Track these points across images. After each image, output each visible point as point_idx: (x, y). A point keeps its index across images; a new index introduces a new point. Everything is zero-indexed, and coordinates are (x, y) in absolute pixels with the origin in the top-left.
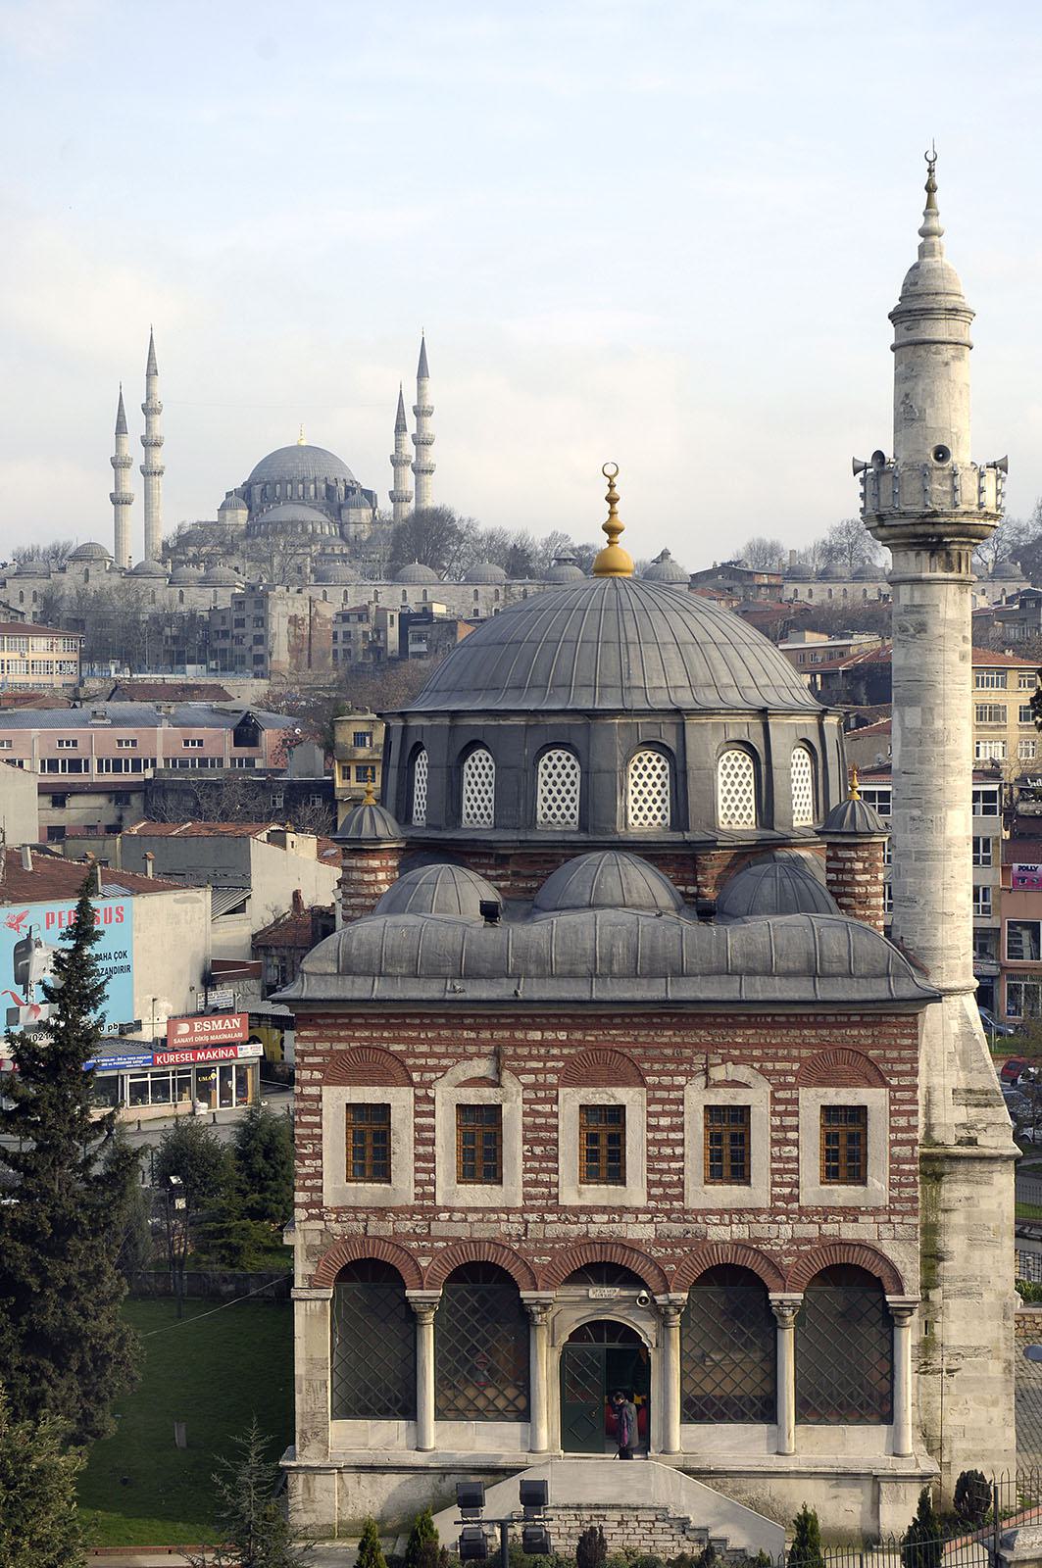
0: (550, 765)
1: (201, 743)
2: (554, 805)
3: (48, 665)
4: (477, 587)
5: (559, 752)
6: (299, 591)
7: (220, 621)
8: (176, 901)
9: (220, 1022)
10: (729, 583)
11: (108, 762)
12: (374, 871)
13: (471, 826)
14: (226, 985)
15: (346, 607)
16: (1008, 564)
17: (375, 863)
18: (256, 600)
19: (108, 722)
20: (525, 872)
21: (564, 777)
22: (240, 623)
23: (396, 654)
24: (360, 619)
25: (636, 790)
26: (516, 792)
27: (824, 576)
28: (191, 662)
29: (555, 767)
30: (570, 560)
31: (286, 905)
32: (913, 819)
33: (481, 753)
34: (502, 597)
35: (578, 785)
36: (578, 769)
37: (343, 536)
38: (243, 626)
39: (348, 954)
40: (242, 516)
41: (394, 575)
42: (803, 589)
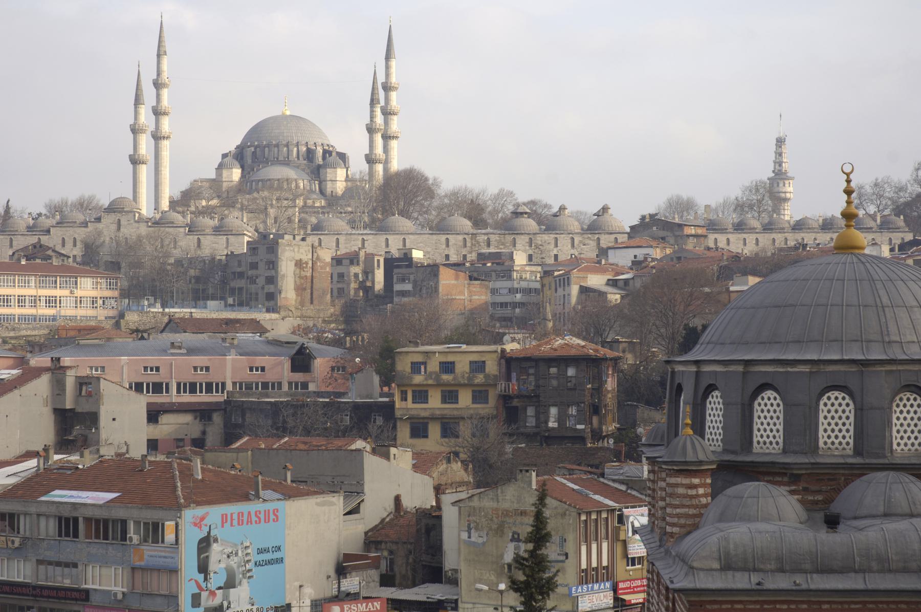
0: (829, 403)
1: (263, 369)
2: (833, 435)
3: (94, 301)
4: (448, 236)
5: (836, 393)
6: (303, 239)
7: (236, 264)
8: (317, 504)
9: (364, 605)
10: (662, 233)
11: (185, 385)
12: (695, 487)
13: (761, 451)
14: (354, 574)
15: (339, 253)
16: (893, 217)
17: (696, 481)
18: (266, 247)
19: (183, 351)
20: (813, 488)
21: (840, 413)
22: (254, 266)
23: (382, 292)
24: (352, 263)
25: (898, 423)
26: (800, 424)
27: (740, 227)
28: (214, 298)
29: (833, 405)
30: (526, 213)
31: (390, 505)
33: (770, 393)
34: (469, 244)
35: (852, 419)
36: (852, 406)
37: (322, 192)
38: (257, 268)
39: (727, 554)
40: (236, 174)
41: (379, 227)
42: (722, 239)
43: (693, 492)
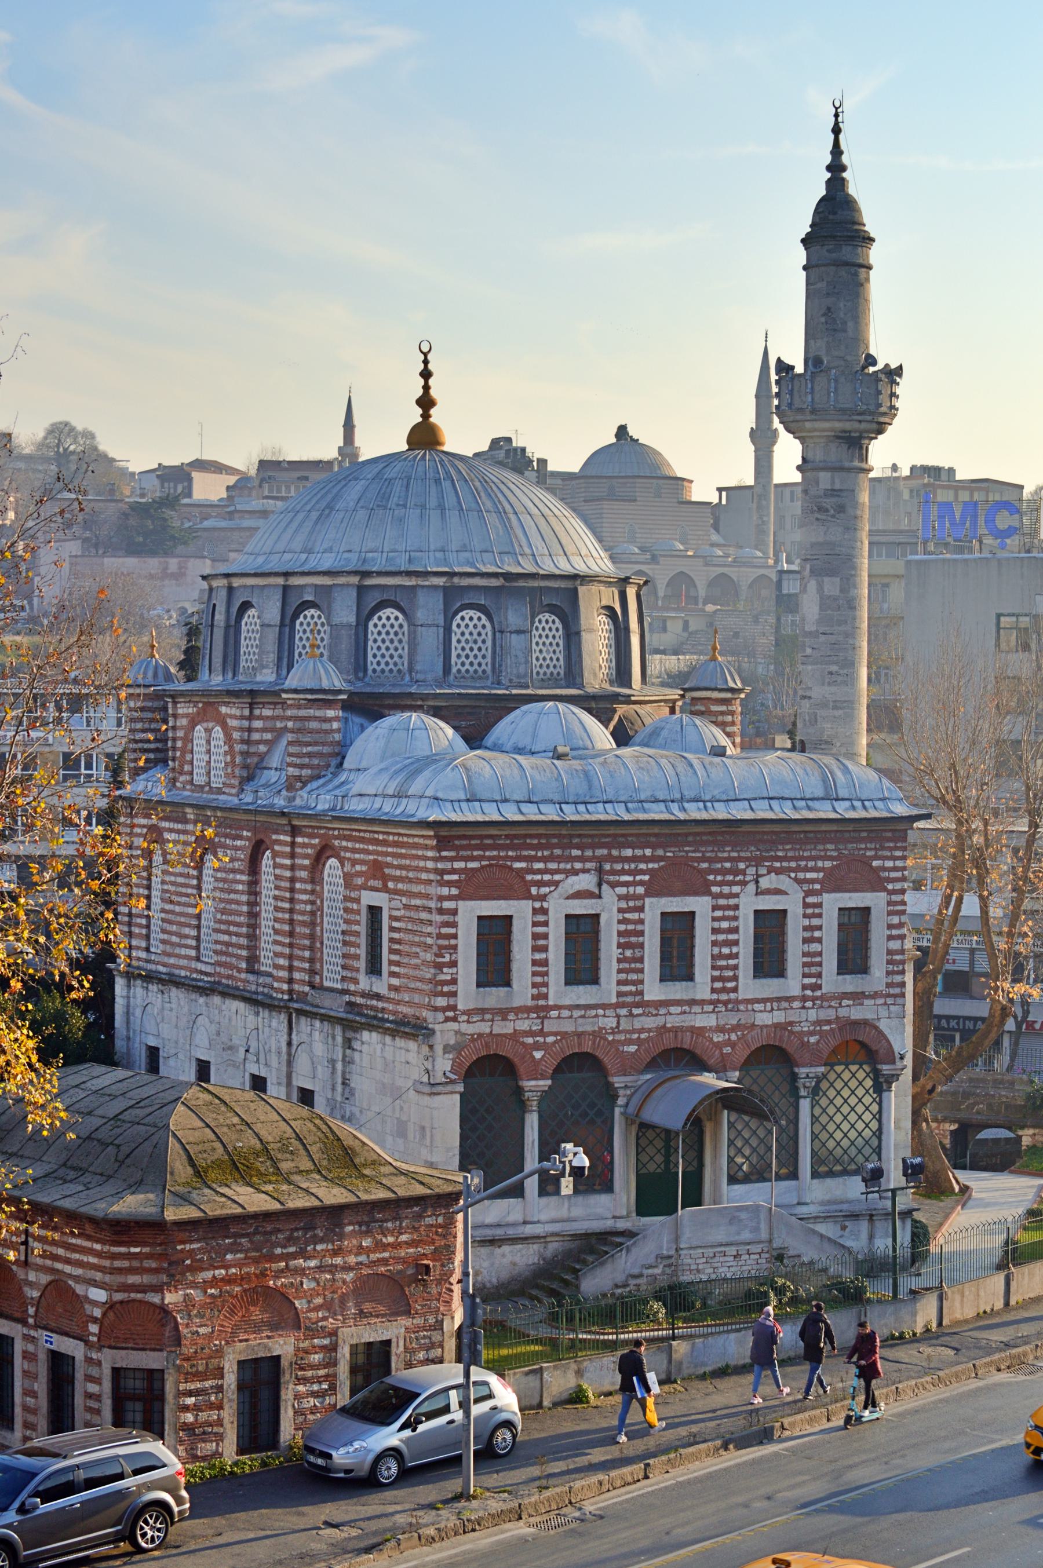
5: (471, 613)
32: (831, 673)
43: (326, 726)
